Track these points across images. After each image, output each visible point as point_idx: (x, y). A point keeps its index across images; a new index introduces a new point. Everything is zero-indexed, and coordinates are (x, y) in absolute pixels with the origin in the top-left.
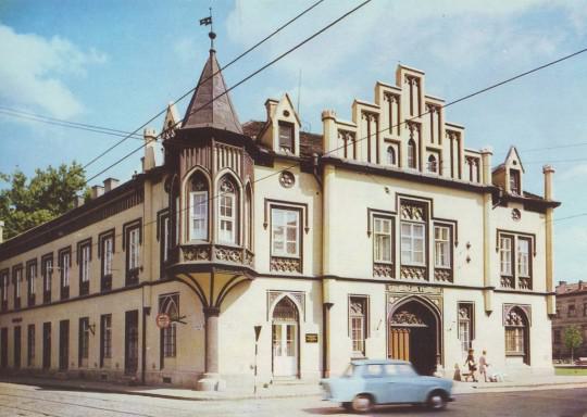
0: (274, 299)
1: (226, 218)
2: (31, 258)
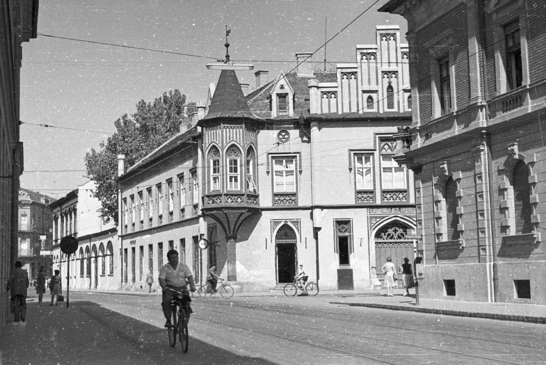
0: (277, 226)
1: (233, 174)
2: (467, 128)
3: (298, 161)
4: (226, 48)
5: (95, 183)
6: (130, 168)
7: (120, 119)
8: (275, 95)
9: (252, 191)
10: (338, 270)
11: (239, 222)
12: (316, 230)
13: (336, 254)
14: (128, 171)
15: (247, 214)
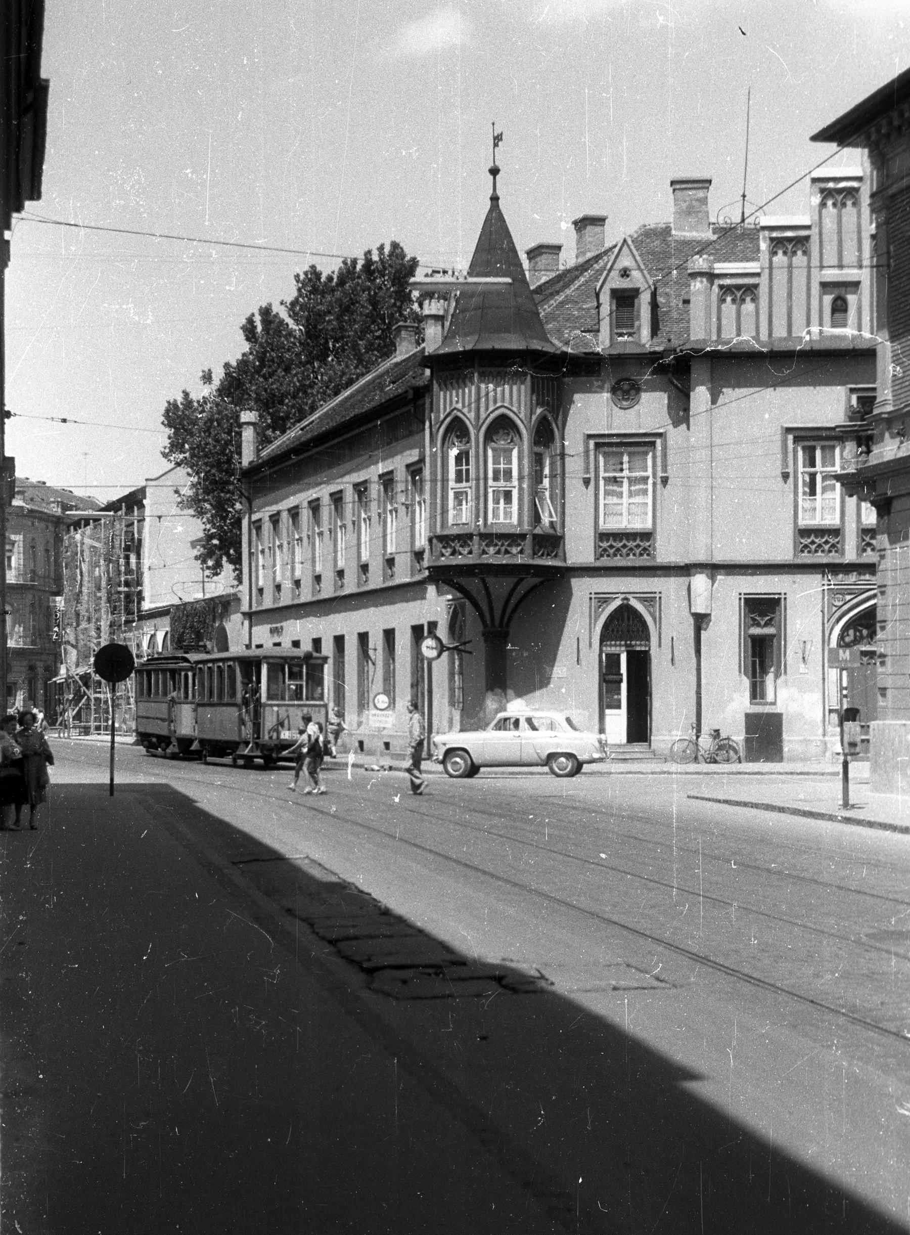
3: (659, 453)
4: (492, 177)
5: (189, 474)
6: (281, 441)
7: (253, 315)
8: (608, 292)
9: (547, 524)
10: (747, 716)
11: (513, 601)
12: (701, 621)
13: (743, 676)
14: (264, 454)
15: (531, 581)
